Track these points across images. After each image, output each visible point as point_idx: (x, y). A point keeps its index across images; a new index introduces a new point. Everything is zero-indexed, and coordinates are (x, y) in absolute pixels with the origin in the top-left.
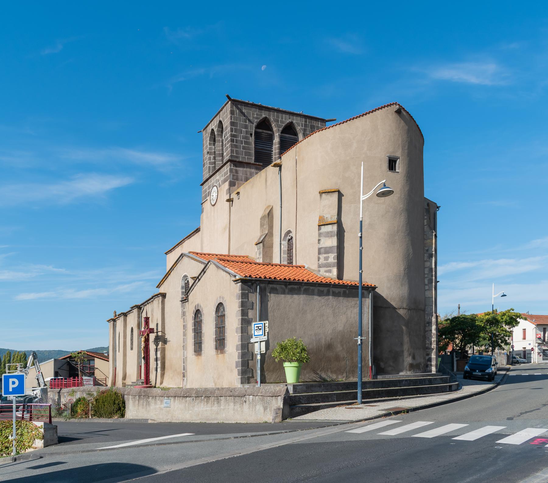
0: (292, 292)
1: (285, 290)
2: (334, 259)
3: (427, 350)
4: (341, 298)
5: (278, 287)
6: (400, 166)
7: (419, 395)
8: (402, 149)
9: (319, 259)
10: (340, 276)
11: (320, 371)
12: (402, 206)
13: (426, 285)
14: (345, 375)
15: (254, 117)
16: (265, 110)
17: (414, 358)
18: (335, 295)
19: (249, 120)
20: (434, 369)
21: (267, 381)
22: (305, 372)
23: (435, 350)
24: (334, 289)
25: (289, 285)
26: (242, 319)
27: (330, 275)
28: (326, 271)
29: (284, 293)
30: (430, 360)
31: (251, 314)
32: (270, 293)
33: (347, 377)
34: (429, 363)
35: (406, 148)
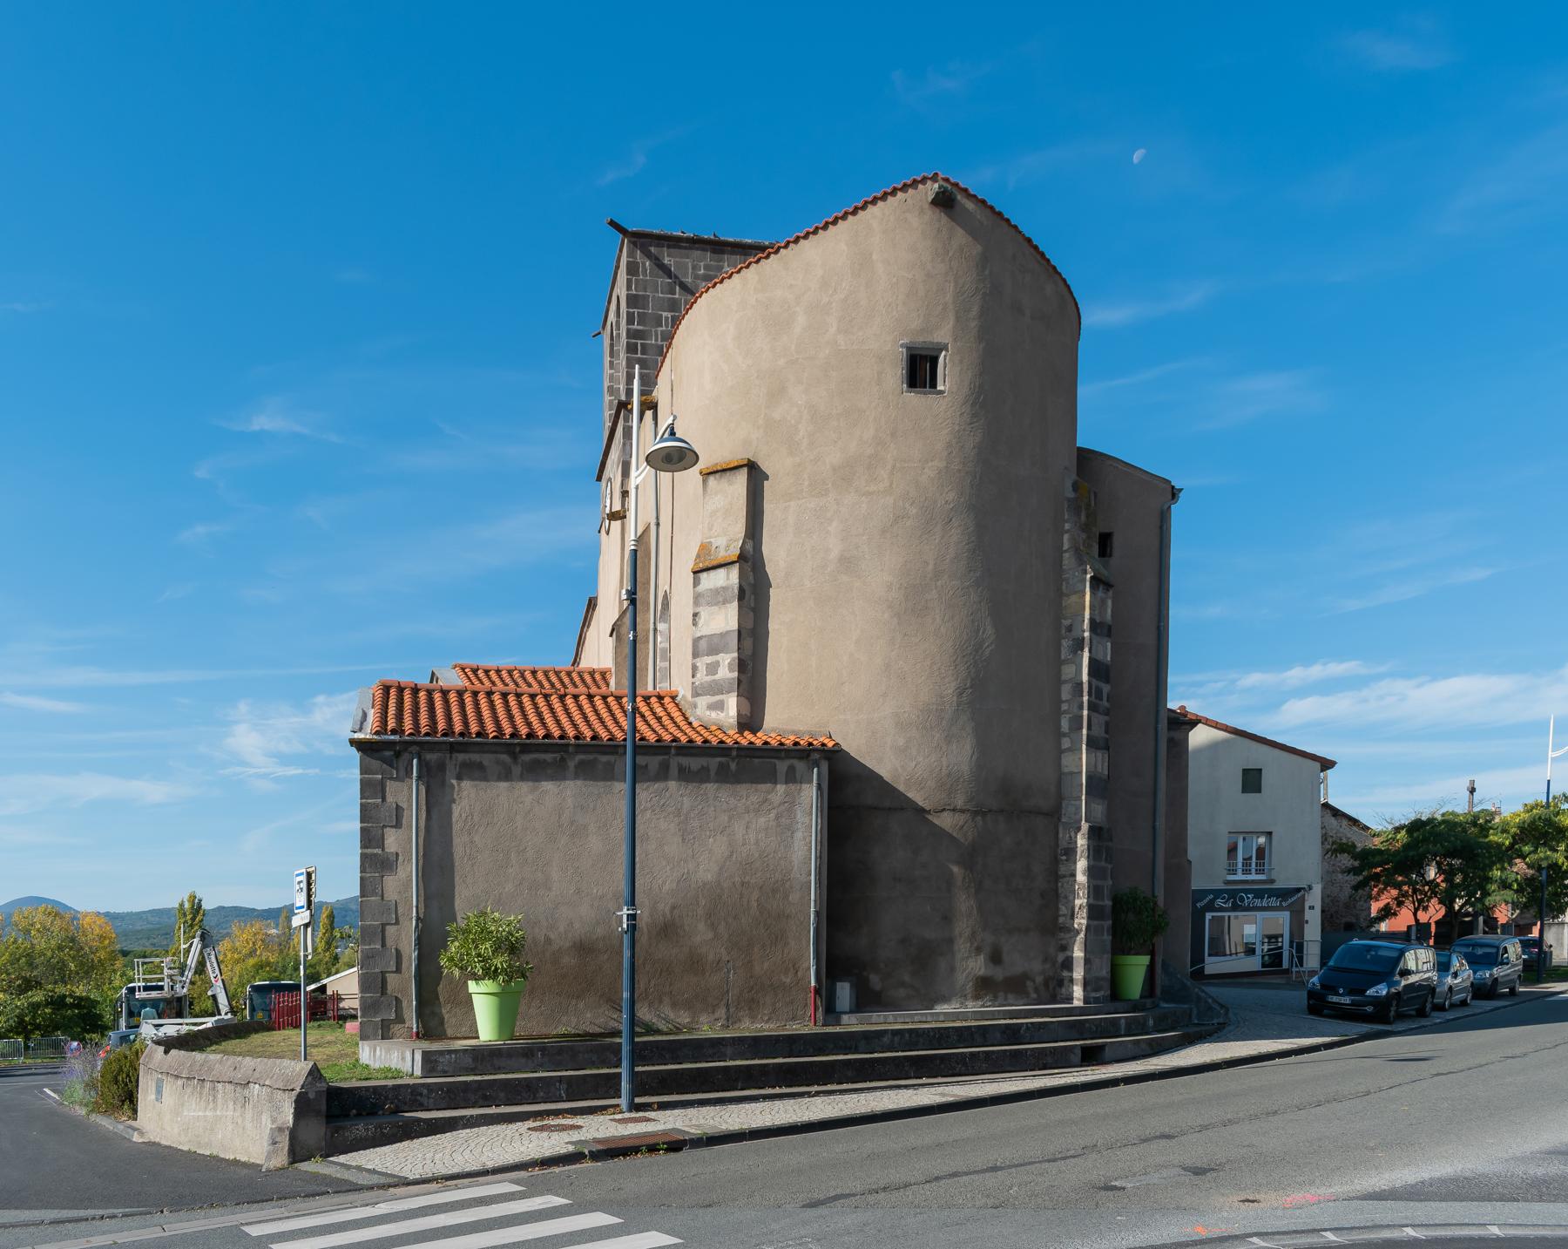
0: (535, 772)
2: (731, 670)
3: (1055, 929)
4: (710, 787)
5: (487, 759)
6: (949, 374)
7: (924, 1080)
8: (958, 319)
9: (694, 668)
10: (750, 721)
12: (951, 496)
13: (1065, 735)
14: (721, 1012)
15: (696, 277)
16: (732, 253)
17: (996, 958)
18: (686, 776)
19: (684, 287)
20: (1078, 992)
21: (449, 1032)
22: (581, 1005)
23: (1082, 935)
24: (685, 761)
25: (522, 752)
26: (363, 856)
27: (722, 715)
28: (711, 707)
29: (506, 776)
30: (1068, 964)
31: (392, 841)
32: (459, 778)
33: (730, 1021)
34: (1065, 974)
35: (975, 310)
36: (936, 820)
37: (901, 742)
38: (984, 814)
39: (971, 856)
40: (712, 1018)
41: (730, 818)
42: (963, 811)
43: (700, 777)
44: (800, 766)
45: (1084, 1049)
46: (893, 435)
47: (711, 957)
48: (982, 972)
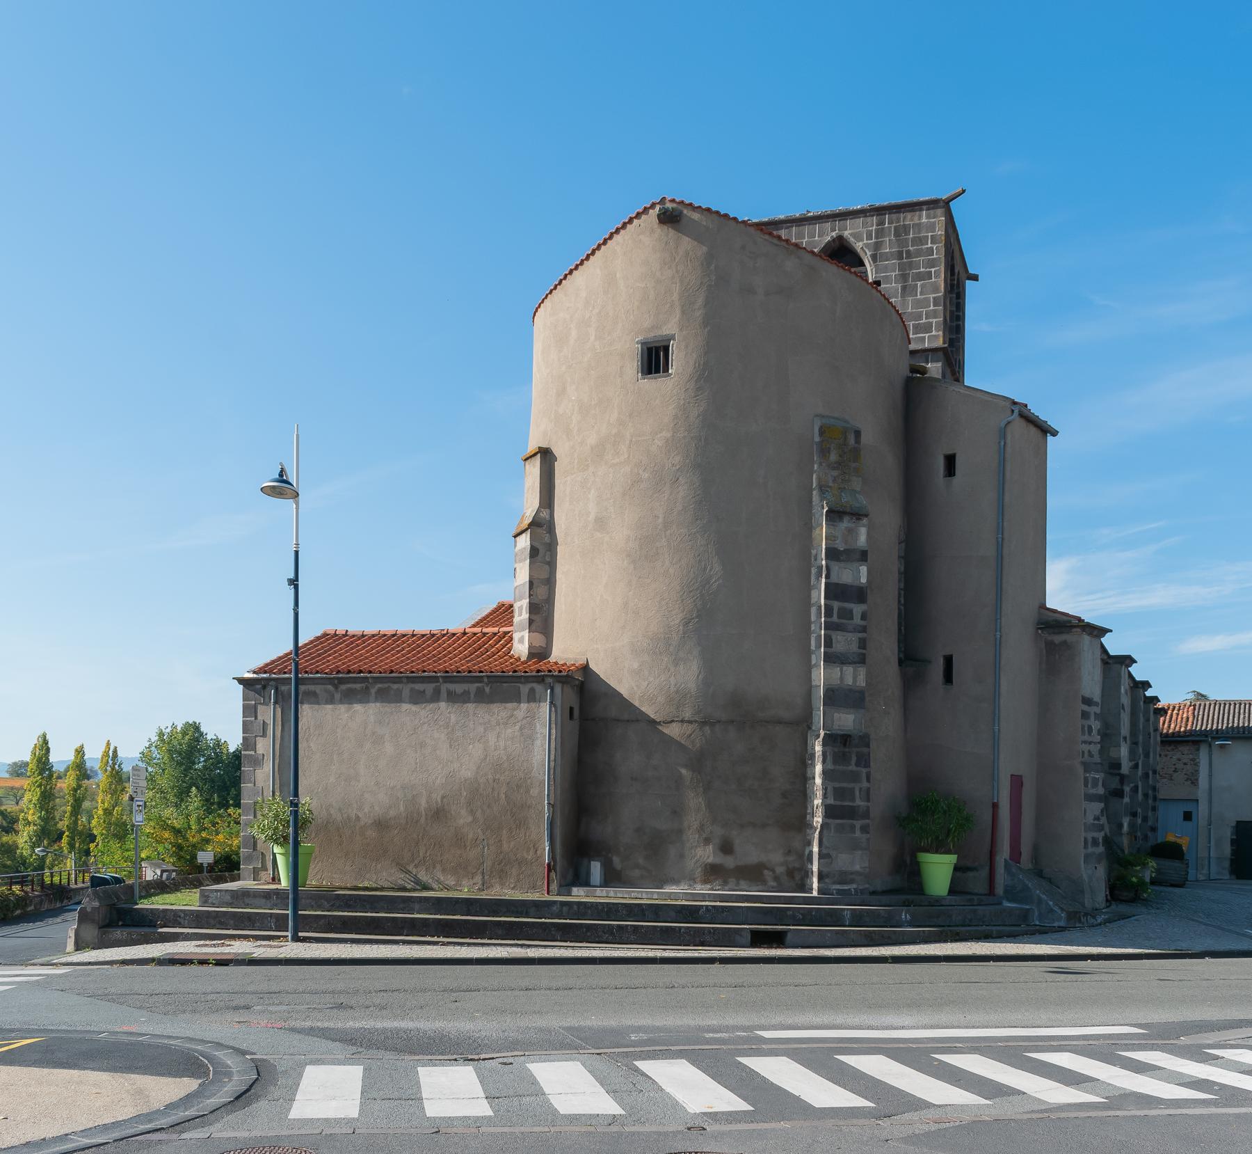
0: (350, 697)
1: (333, 696)
3: (801, 824)
4: (471, 706)
5: (318, 689)
6: (679, 360)
8: (683, 312)
11: (416, 866)
14: (478, 879)
17: (726, 848)
18: (453, 698)
24: (452, 687)
29: (331, 701)
33: (485, 886)
35: (700, 301)
36: (666, 730)
37: (636, 665)
38: (712, 725)
39: (698, 762)
40: (471, 882)
41: (485, 730)
42: (690, 722)
43: (463, 698)
44: (538, 688)
45: (755, 933)
46: (630, 415)
47: (470, 836)
48: (711, 860)
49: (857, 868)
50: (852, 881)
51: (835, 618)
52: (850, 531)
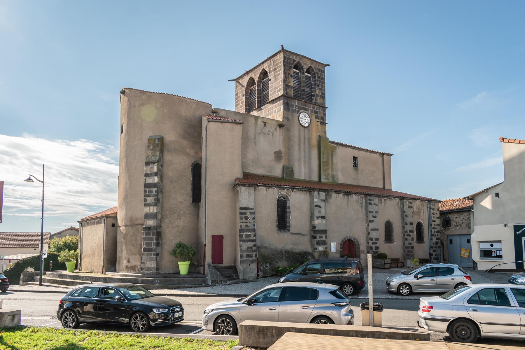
45: (284, 290)
49: (153, 266)
50: (151, 270)
51: (147, 193)
52: (152, 168)
